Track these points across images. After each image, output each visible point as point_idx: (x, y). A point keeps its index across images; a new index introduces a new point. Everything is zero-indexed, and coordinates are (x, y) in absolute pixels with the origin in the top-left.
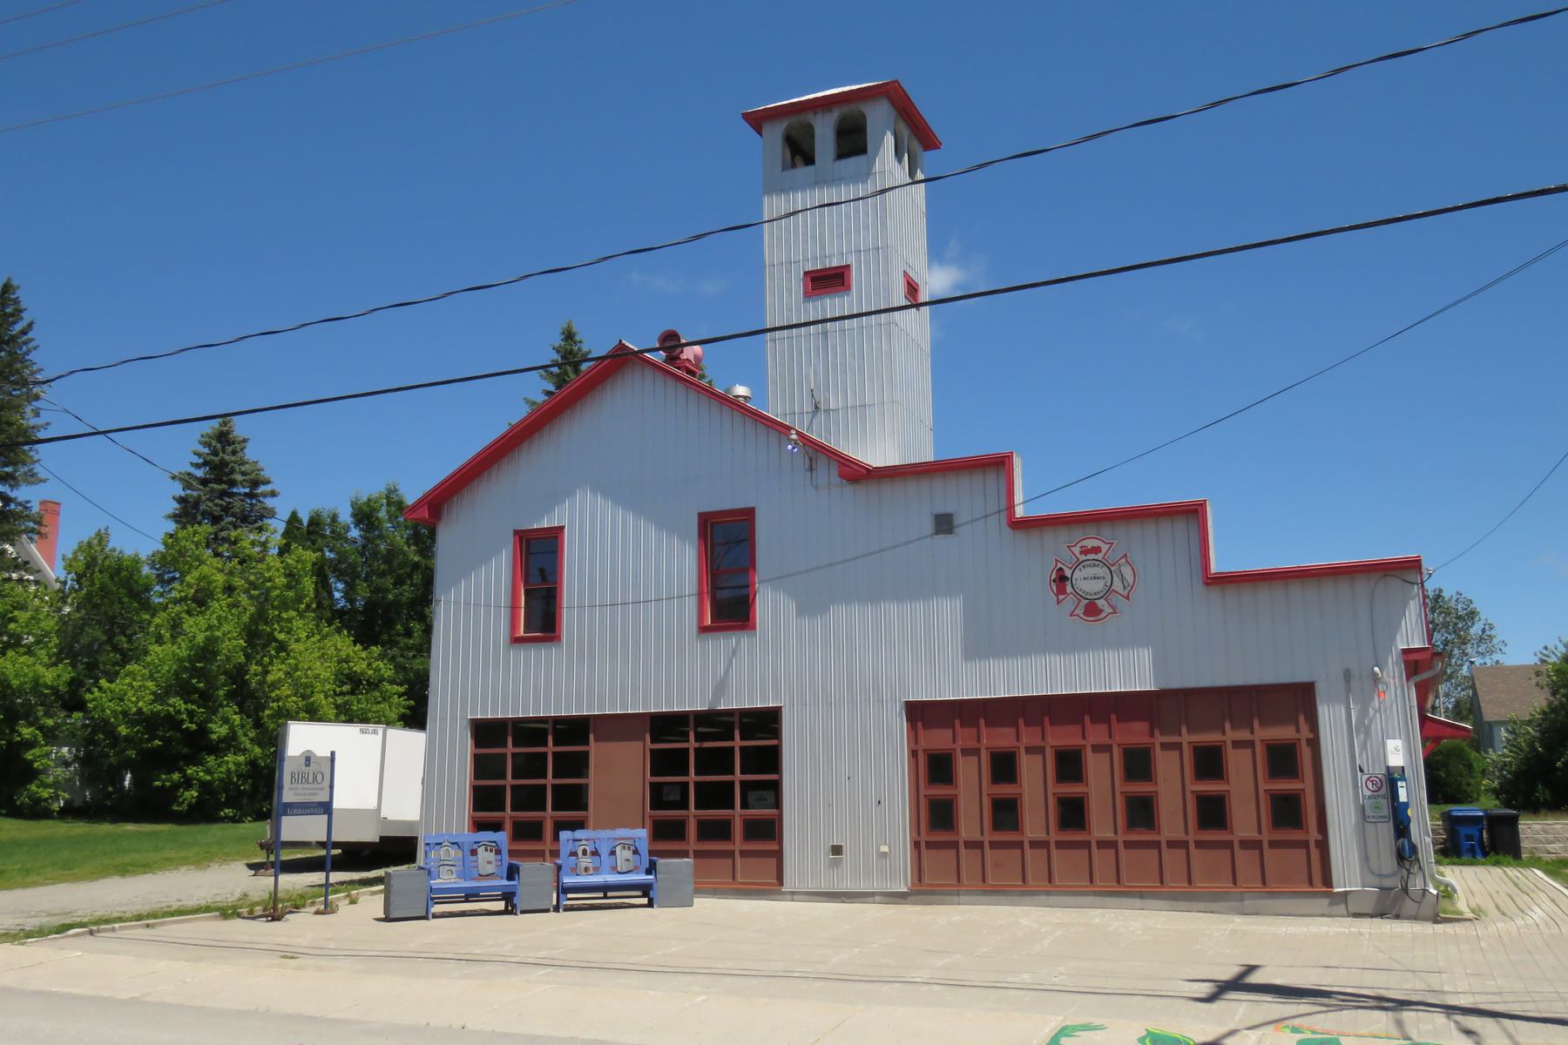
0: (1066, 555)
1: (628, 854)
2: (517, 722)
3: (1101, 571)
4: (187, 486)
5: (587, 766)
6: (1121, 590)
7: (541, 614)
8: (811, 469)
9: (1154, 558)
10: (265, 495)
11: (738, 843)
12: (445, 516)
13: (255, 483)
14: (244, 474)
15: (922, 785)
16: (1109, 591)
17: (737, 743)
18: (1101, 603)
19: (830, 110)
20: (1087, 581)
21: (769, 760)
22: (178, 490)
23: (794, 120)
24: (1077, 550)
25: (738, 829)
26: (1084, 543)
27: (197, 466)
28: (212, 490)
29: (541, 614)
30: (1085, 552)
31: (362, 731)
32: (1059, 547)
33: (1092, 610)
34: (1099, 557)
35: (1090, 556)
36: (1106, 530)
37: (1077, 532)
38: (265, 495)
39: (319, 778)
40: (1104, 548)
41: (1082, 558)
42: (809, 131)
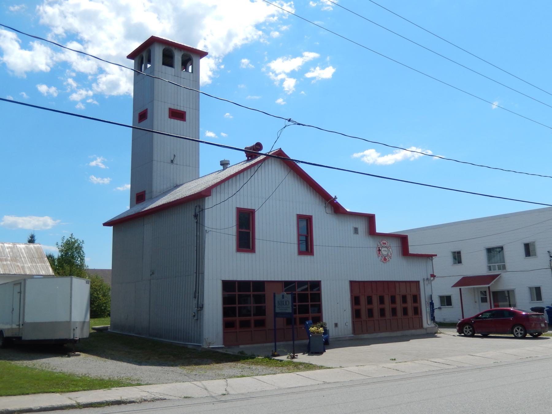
3: (386, 249)
7: (246, 240)
19: (181, 51)
20: (384, 251)
21: (317, 297)
25: (238, 324)
29: (246, 240)
30: (384, 244)
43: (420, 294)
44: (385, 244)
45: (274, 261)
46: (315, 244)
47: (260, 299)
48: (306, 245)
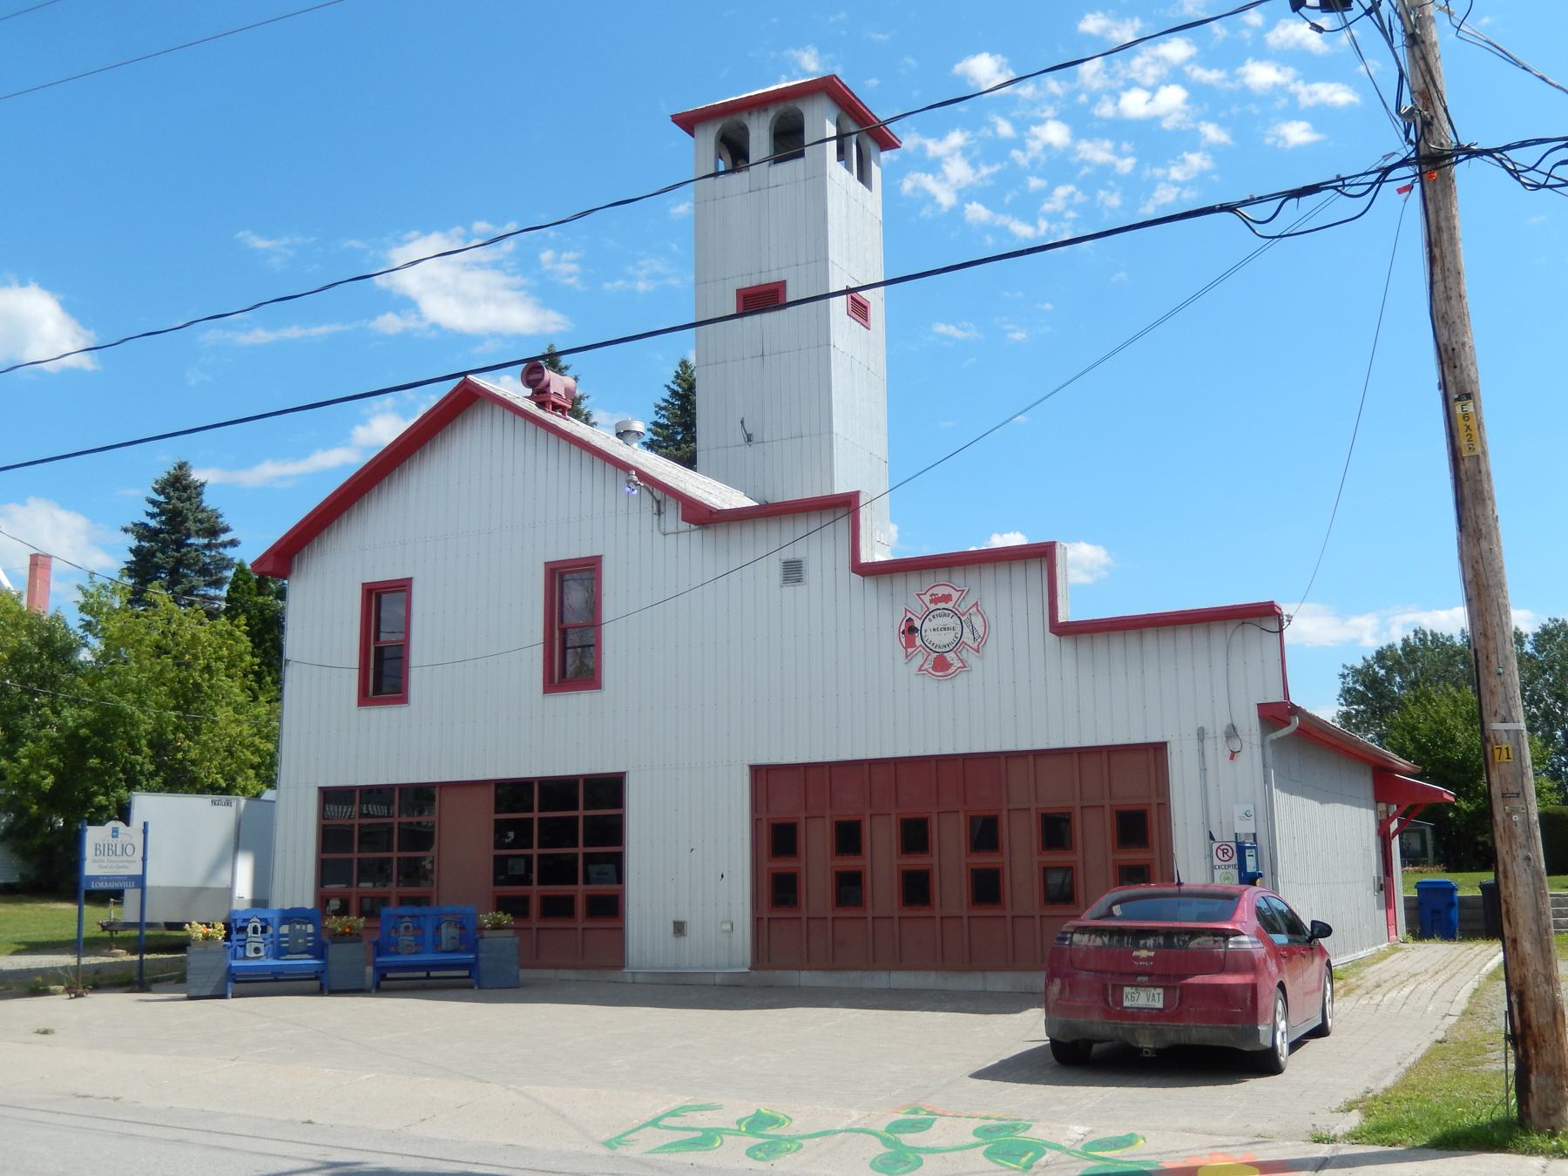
0: (917, 608)
1: (454, 932)
2: (403, 788)
3: (951, 622)
4: (140, 538)
5: (431, 844)
6: (970, 642)
7: (384, 675)
8: (659, 513)
9: (1008, 608)
10: (224, 545)
11: (580, 919)
12: (295, 572)
13: (213, 531)
14: (201, 521)
15: (1080, 865)
16: (959, 643)
17: (581, 813)
18: (950, 657)
19: (766, 110)
20: (937, 632)
21: (611, 832)
22: (132, 542)
23: (727, 120)
24: (927, 598)
25: (580, 907)
26: (934, 591)
27: (153, 516)
28: (164, 541)
29: (384, 675)
30: (935, 600)
31: (214, 803)
32: (911, 596)
33: (941, 664)
34: (950, 605)
35: (941, 605)
36: (958, 578)
37: (928, 579)
38: (224, 545)
39: (129, 850)
40: (955, 595)
41: (932, 607)
42: (744, 131)
43: (1164, 806)
44: (947, 598)
45: (479, 721)
46: (355, 674)
47: (420, 838)
48: (571, 658)
